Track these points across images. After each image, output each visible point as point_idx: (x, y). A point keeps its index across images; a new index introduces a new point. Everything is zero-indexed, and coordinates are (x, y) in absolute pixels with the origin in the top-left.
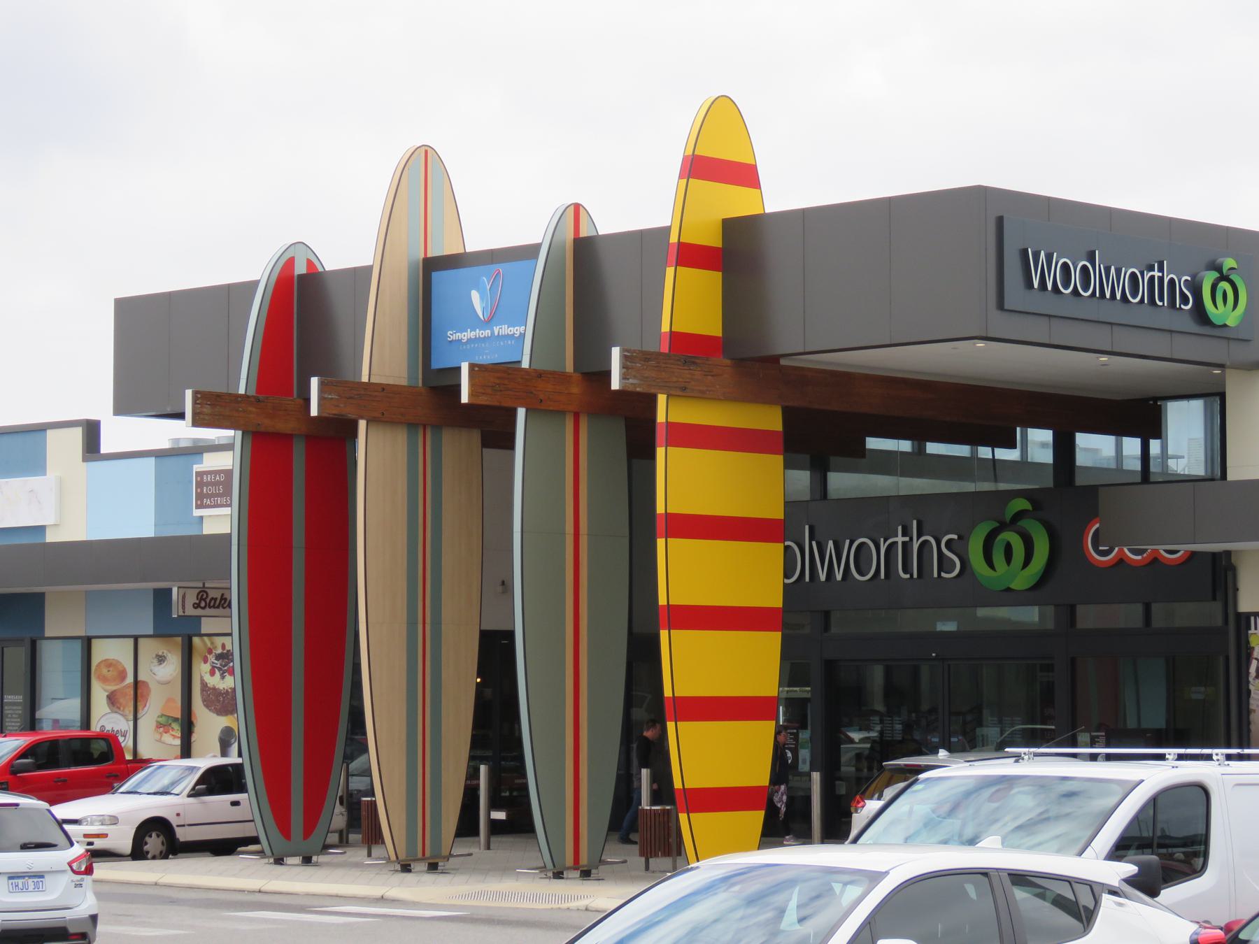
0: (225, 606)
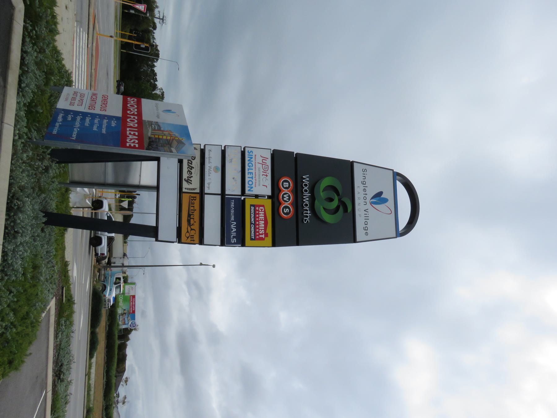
0: (189, 169)
